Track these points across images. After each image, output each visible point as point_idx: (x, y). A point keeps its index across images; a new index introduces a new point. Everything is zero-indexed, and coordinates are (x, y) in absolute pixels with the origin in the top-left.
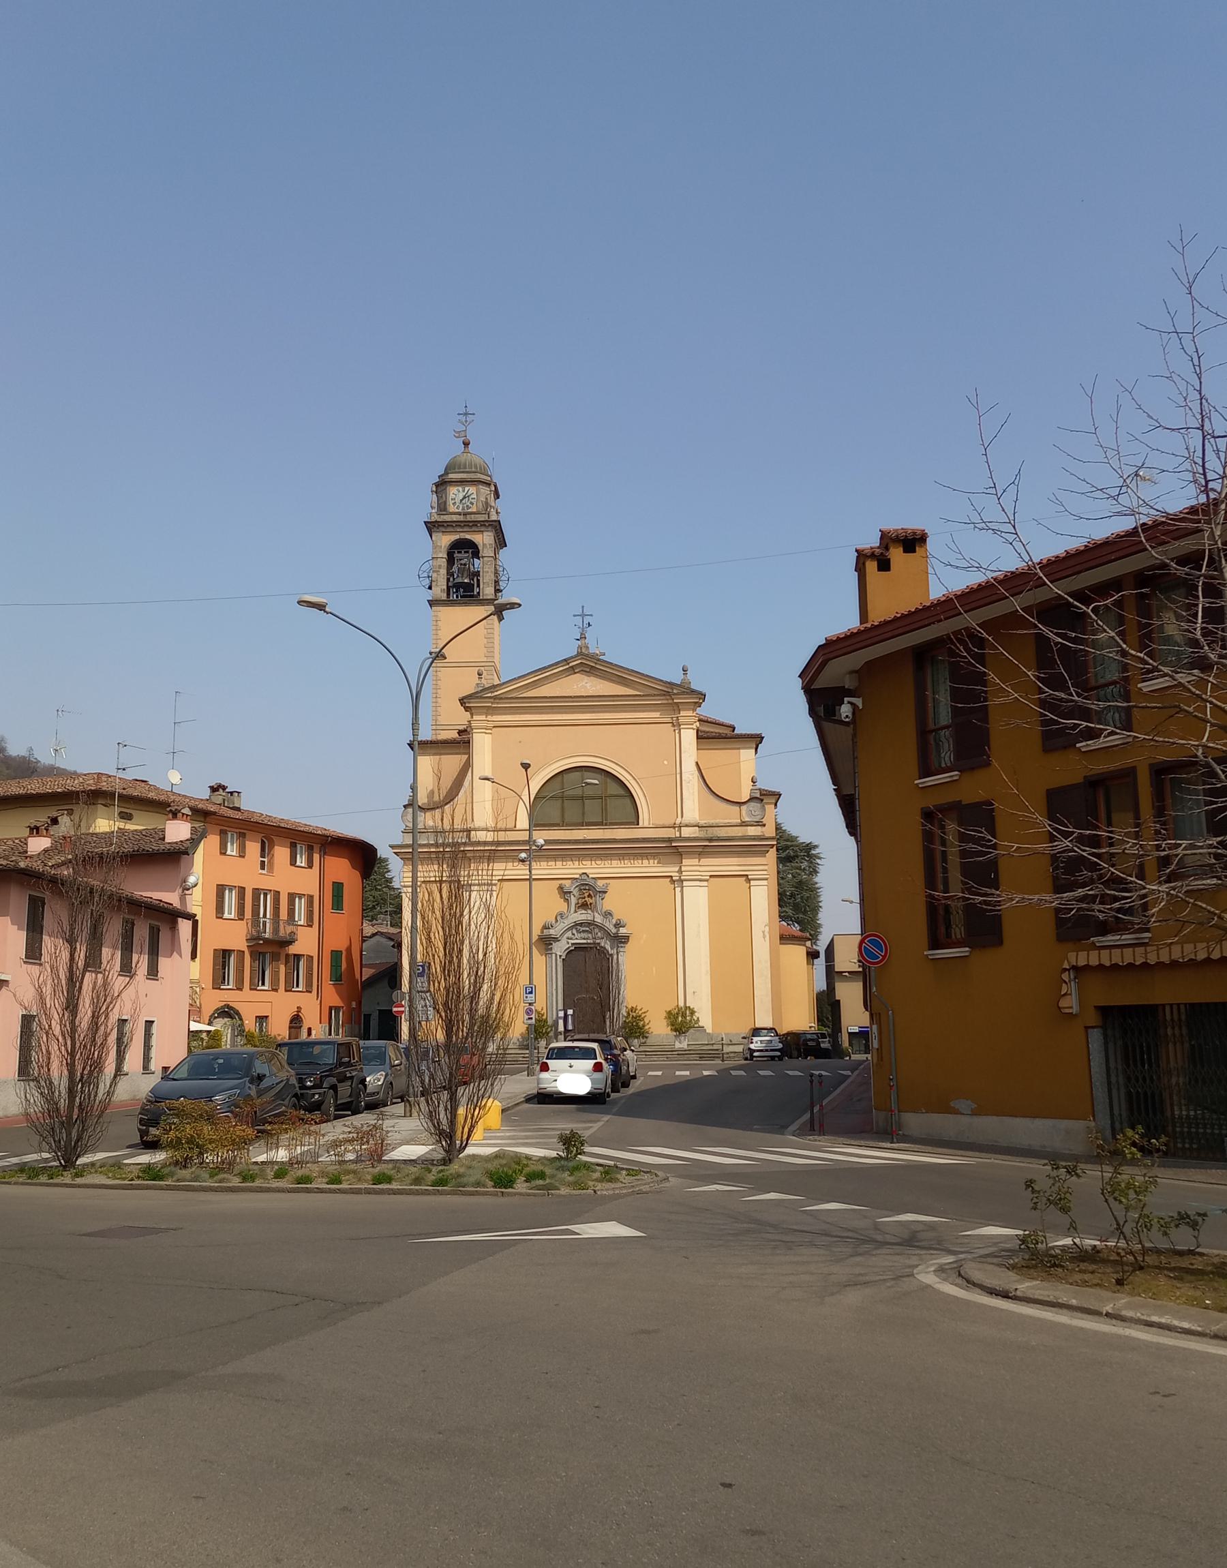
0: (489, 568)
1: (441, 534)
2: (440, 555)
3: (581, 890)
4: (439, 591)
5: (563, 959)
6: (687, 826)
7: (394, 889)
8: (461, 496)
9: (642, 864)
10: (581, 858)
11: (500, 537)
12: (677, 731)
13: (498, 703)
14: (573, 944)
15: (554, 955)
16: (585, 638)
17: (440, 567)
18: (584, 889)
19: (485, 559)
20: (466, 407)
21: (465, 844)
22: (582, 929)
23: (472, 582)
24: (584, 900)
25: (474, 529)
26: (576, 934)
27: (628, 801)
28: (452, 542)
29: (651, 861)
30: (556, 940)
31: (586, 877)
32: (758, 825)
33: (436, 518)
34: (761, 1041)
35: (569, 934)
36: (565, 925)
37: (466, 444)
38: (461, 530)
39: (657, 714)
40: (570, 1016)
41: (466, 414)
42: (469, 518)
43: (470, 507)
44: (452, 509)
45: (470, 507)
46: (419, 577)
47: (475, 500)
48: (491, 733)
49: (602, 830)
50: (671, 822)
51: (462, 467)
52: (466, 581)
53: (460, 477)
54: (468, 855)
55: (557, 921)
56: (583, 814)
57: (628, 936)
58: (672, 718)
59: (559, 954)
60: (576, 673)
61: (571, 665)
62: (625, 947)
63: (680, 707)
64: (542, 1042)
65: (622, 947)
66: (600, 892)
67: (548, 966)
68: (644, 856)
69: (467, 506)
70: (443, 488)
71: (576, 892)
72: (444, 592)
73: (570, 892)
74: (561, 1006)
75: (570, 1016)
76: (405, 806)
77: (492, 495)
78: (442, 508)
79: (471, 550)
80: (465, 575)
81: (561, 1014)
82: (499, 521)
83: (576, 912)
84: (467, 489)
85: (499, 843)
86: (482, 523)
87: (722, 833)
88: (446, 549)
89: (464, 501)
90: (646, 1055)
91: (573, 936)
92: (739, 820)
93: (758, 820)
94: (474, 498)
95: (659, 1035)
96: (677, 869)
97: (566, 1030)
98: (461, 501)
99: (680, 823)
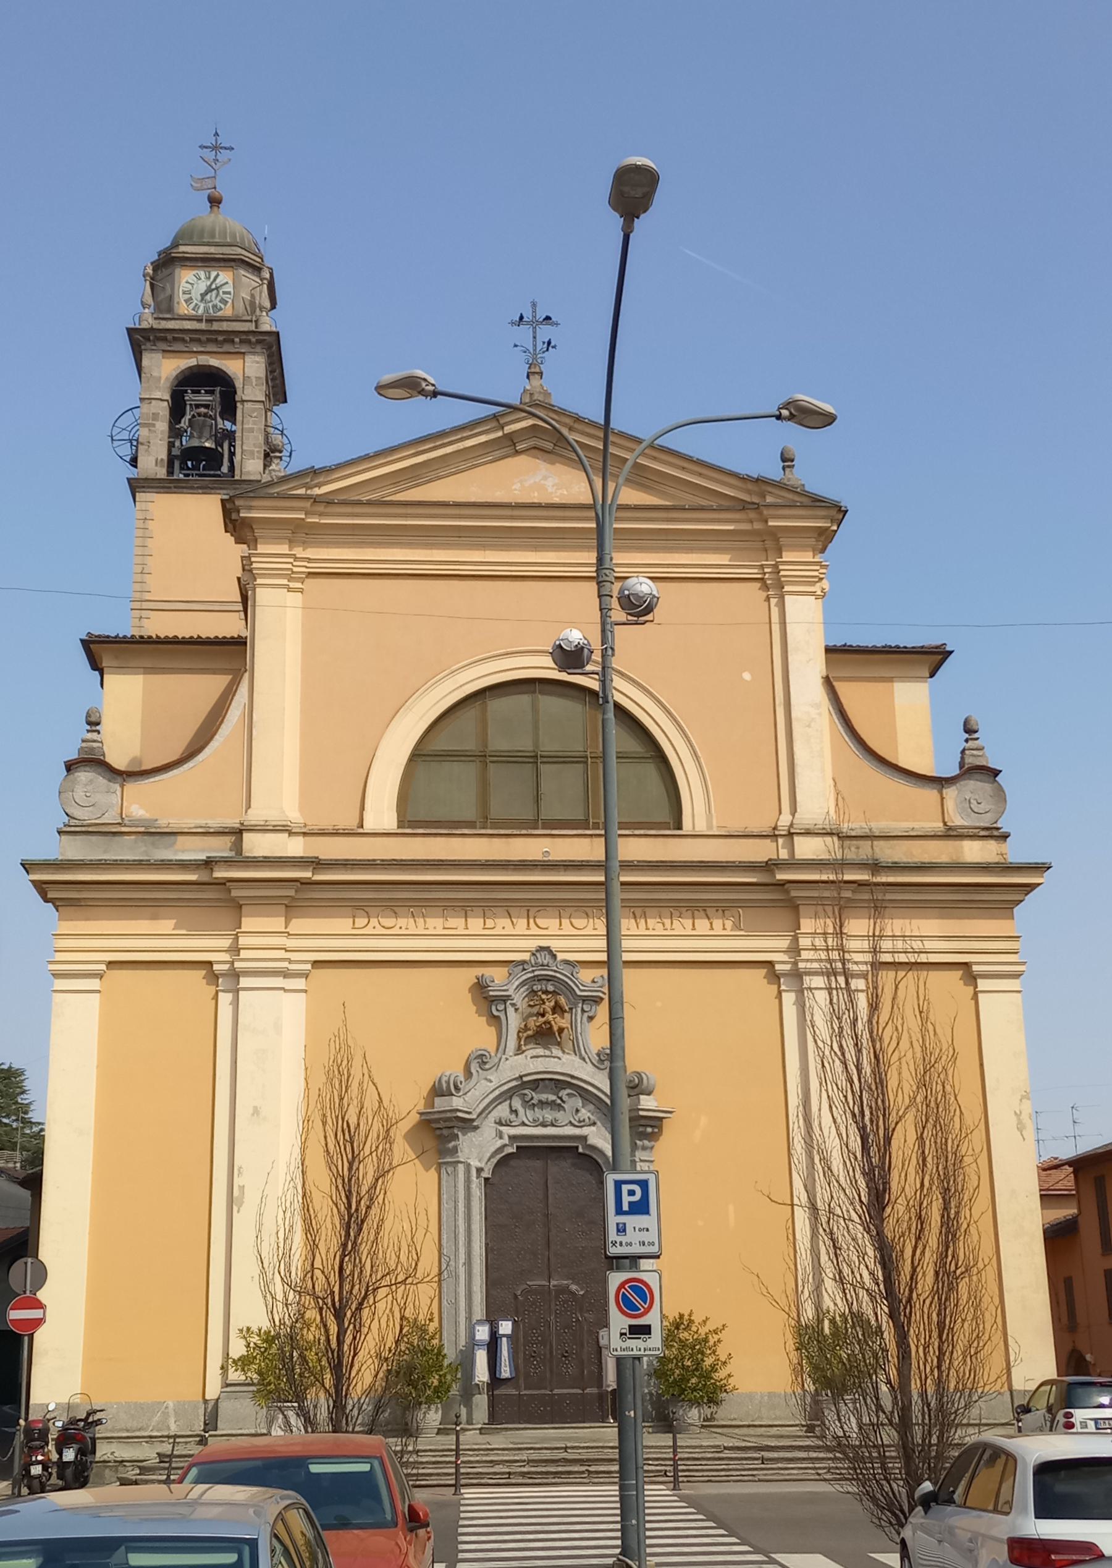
0: (254, 423)
1: (160, 355)
2: (158, 395)
3: (534, 992)
4: (154, 461)
5: (486, 1179)
6: (808, 833)
7: (31, 1122)
8: (202, 286)
9: (694, 928)
10: (533, 911)
11: (278, 382)
12: (773, 601)
13: (321, 515)
14: (513, 1138)
15: (461, 1167)
16: (541, 374)
17: (155, 416)
18: (546, 992)
19: (248, 405)
20: (216, 134)
21: (227, 862)
22: (537, 1097)
23: (219, 449)
24: (541, 1020)
25: (227, 347)
26: (521, 1111)
27: (650, 770)
28: (182, 371)
29: (718, 923)
30: (468, 1125)
31: (547, 959)
32: (991, 837)
33: (148, 322)
34: (1096, 1420)
35: (503, 1111)
36: (492, 1086)
37: (215, 202)
38: (202, 349)
39: (724, 559)
40: (504, 1340)
41: (215, 148)
42: (216, 326)
43: (221, 309)
44: (183, 309)
45: (221, 309)
46: (112, 440)
47: (232, 297)
48: (301, 591)
49: (587, 840)
50: (762, 825)
51: (206, 235)
52: (207, 445)
53: (201, 251)
54: (234, 893)
55: (468, 1074)
56: (537, 800)
57: (661, 1119)
58: (762, 567)
59: (475, 1163)
60: (517, 453)
61: (508, 429)
62: (652, 1148)
63: (783, 541)
64: (432, 1413)
65: (644, 1148)
66: (585, 1000)
67: (445, 1197)
68: (697, 908)
69: (214, 306)
70: (166, 272)
71: (519, 998)
72: (162, 466)
73: (504, 999)
74: (479, 1312)
75: (504, 1340)
76: (70, 767)
77: (265, 286)
78: (164, 305)
79: (218, 389)
80: (206, 433)
81: (483, 1333)
82: (278, 334)
83: (519, 1051)
84: (213, 274)
85: (317, 864)
86: (244, 337)
87: (889, 852)
88: (168, 385)
89: (208, 297)
90: (763, 1460)
91: (513, 1117)
92: (941, 825)
93: (987, 825)
94: (229, 293)
95: (751, 1396)
96: (784, 944)
97: (495, 1380)
98: (203, 295)
99: (792, 825)
